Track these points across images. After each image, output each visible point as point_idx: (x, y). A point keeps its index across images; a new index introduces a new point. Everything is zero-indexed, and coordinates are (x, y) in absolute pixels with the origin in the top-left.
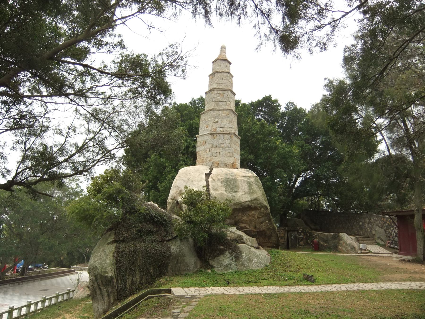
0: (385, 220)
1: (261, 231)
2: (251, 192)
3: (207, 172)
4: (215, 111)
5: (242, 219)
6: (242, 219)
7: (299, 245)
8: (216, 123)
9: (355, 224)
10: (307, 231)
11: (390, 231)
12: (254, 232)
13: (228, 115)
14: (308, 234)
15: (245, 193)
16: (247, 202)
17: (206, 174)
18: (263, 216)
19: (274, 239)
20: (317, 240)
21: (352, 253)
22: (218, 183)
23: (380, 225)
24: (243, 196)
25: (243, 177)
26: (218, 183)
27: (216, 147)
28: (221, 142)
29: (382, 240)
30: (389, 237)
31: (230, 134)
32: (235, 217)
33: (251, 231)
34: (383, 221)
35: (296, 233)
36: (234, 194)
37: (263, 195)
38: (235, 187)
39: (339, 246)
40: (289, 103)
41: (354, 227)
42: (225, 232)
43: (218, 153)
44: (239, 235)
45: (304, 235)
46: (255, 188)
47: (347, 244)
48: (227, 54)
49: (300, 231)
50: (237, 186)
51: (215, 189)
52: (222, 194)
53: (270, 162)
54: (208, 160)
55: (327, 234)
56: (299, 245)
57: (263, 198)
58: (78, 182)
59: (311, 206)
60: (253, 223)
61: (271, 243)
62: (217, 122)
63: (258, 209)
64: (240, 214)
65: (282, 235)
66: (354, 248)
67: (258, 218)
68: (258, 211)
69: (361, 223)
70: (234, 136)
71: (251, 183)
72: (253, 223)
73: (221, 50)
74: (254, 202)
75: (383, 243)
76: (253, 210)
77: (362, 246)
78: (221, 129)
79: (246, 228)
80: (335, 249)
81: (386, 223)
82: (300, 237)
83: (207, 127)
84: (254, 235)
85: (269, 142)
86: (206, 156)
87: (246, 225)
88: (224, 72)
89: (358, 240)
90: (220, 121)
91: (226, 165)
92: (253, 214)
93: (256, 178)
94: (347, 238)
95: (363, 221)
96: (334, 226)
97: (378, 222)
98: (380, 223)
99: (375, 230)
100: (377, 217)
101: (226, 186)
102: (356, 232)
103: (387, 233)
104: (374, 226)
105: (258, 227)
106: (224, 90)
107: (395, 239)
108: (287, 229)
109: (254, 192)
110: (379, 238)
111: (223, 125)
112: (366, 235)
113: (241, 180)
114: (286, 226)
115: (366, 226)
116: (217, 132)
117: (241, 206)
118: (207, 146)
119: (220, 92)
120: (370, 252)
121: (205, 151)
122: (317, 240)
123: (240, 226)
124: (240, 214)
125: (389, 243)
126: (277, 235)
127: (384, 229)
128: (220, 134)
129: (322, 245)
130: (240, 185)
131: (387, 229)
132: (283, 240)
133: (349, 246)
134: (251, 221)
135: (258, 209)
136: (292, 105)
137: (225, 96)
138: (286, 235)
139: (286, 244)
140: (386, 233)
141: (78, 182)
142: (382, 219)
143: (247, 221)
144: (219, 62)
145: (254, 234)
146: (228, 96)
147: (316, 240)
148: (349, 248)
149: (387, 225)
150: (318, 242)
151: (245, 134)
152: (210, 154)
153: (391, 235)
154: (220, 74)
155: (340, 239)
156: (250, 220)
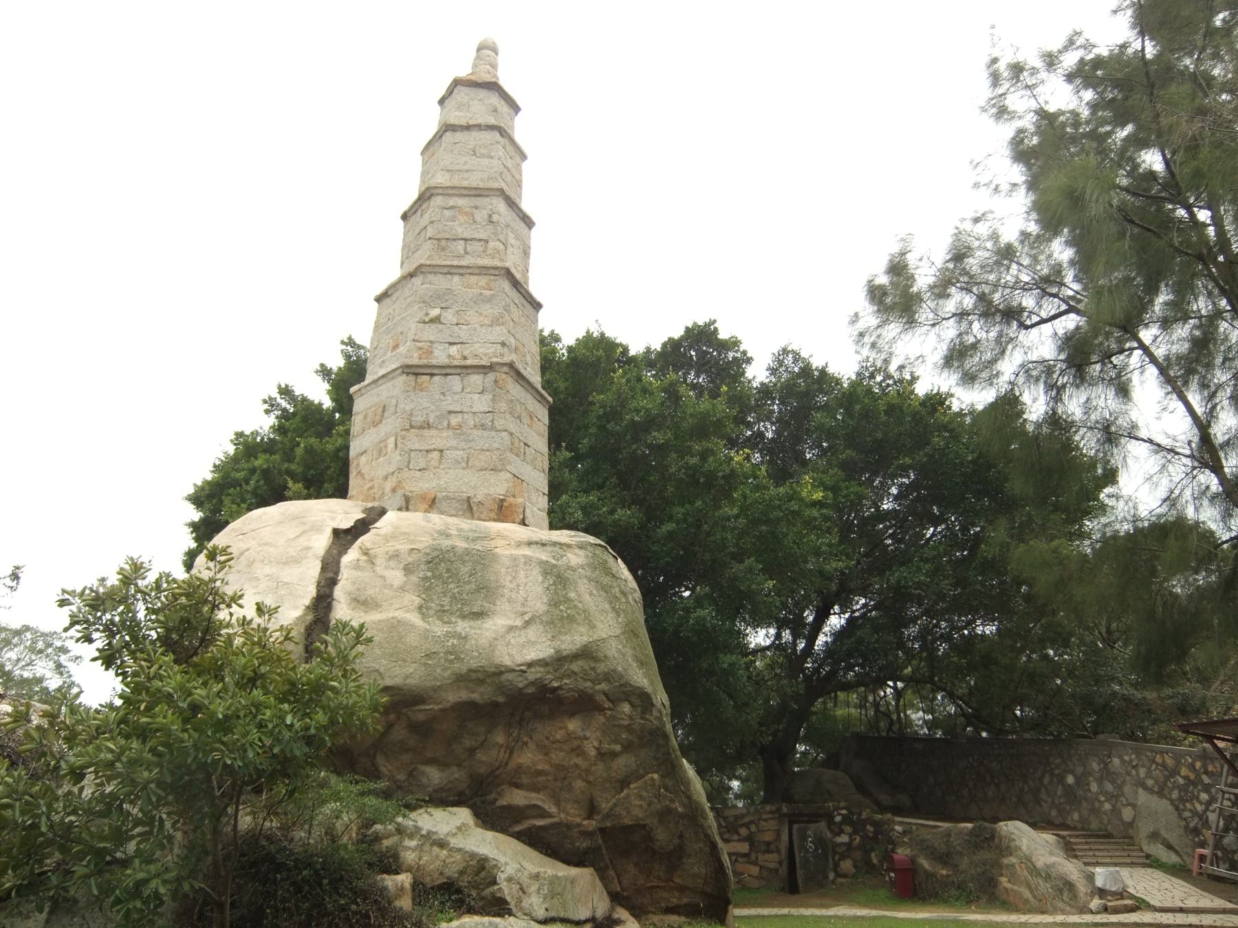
0: (1170, 762)
1: (627, 829)
2: (561, 612)
3: (347, 524)
4: (431, 277)
5: (512, 765)
6: (512, 765)
7: (838, 875)
8: (434, 326)
9: (1046, 780)
10: (864, 815)
11: (1199, 808)
12: (586, 834)
13: (488, 293)
14: (869, 827)
15: (527, 624)
16: (530, 665)
17: (337, 533)
18: (627, 747)
19: (695, 868)
20: (908, 851)
21: (1063, 912)
22: (389, 574)
23: (1150, 782)
24: (512, 636)
25: (530, 544)
26: (389, 574)
27: (427, 425)
28: (449, 403)
29: (1170, 847)
30: (1196, 831)
31: (491, 368)
32: (472, 751)
33: (569, 826)
34: (1164, 765)
35: (823, 825)
36: (462, 626)
37: (630, 632)
38: (479, 589)
39: (1004, 880)
40: (785, 351)
41: (1043, 795)
42: (386, 843)
43: (435, 455)
44: (473, 855)
45: (855, 832)
46: (587, 598)
47: (1034, 871)
48: (499, 74)
49: (838, 819)
50: (487, 590)
51: (360, 602)
52: (395, 625)
53: (708, 534)
54: (388, 486)
55: (945, 825)
56: (838, 875)
57: (629, 652)
58: (63, 659)
59: (873, 724)
60: (579, 784)
61: (682, 889)
62: (436, 320)
63: (601, 710)
64: (500, 738)
65: (768, 837)
66: (1070, 886)
67: (602, 755)
68: (601, 719)
69: (1070, 780)
70: (509, 380)
71: (569, 574)
72: (579, 784)
73: (478, 58)
74: (575, 666)
75: (1174, 859)
76: (572, 714)
77: (1102, 876)
78: (454, 350)
79: (543, 814)
80: (986, 891)
81: (1174, 772)
82: (839, 840)
83: (396, 347)
84: (586, 852)
85: (704, 456)
86: (381, 473)
87: (536, 799)
88: (479, 127)
89: (1070, 850)
90: (449, 316)
91: (469, 508)
92: (570, 736)
93: (598, 551)
94: (1032, 844)
95: (1079, 770)
96: (965, 792)
97: (1142, 772)
98: (1149, 774)
99: (1134, 806)
100: (1138, 753)
101: (426, 587)
102: (1054, 813)
103: (1187, 814)
104: (1127, 789)
105: (605, 806)
106: (478, 192)
107: (1226, 841)
108: (785, 810)
109: (580, 618)
110: (1154, 836)
111: (463, 333)
112: (1094, 825)
113: (514, 559)
114: (789, 799)
115: (1094, 787)
116: (434, 362)
117: (501, 688)
118: (390, 425)
119: (461, 202)
120: (1140, 905)
121: (381, 451)
122: (908, 851)
123: (502, 802)
124: (500, 738)
125: (1202, 858)
126: (714, 846)
127: (1172, 801)
128: (446, 370)
129: (928, 875)
130: (506, 581)
131: (1181, 799)
132: (774, 857)
133: (1048, 877)
134: (563, 774)
135: (601, 710)
136: (796, 360)
137: (481, 216)
138: (785, 837)
139: (783, 871)
140: (1180, 816)
141: (63, 659)
142: (1158, 759)
143: (539, 773)
144: (462, 94)
145: (584, 844)
146: (495, 218)
147: (902, 853)
148: (1044, 887)
149: (1181, 781)
150: (913, 860)
151: (602, 428)
152: (396, 458)
153: (1206, 824)
154: (466, 133)
155: (1004, 848)
156: (559, 767)
